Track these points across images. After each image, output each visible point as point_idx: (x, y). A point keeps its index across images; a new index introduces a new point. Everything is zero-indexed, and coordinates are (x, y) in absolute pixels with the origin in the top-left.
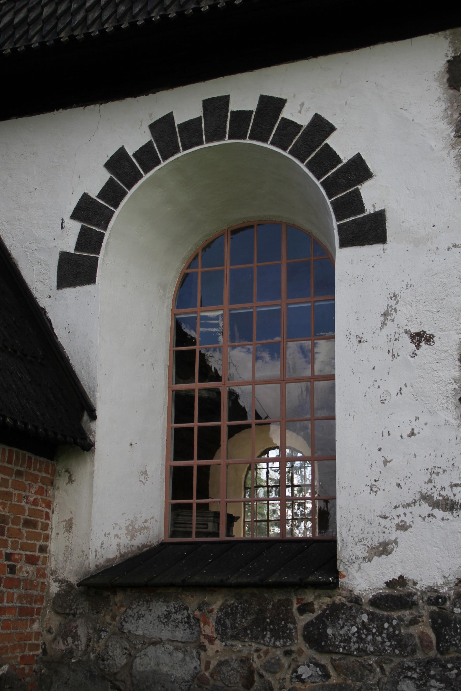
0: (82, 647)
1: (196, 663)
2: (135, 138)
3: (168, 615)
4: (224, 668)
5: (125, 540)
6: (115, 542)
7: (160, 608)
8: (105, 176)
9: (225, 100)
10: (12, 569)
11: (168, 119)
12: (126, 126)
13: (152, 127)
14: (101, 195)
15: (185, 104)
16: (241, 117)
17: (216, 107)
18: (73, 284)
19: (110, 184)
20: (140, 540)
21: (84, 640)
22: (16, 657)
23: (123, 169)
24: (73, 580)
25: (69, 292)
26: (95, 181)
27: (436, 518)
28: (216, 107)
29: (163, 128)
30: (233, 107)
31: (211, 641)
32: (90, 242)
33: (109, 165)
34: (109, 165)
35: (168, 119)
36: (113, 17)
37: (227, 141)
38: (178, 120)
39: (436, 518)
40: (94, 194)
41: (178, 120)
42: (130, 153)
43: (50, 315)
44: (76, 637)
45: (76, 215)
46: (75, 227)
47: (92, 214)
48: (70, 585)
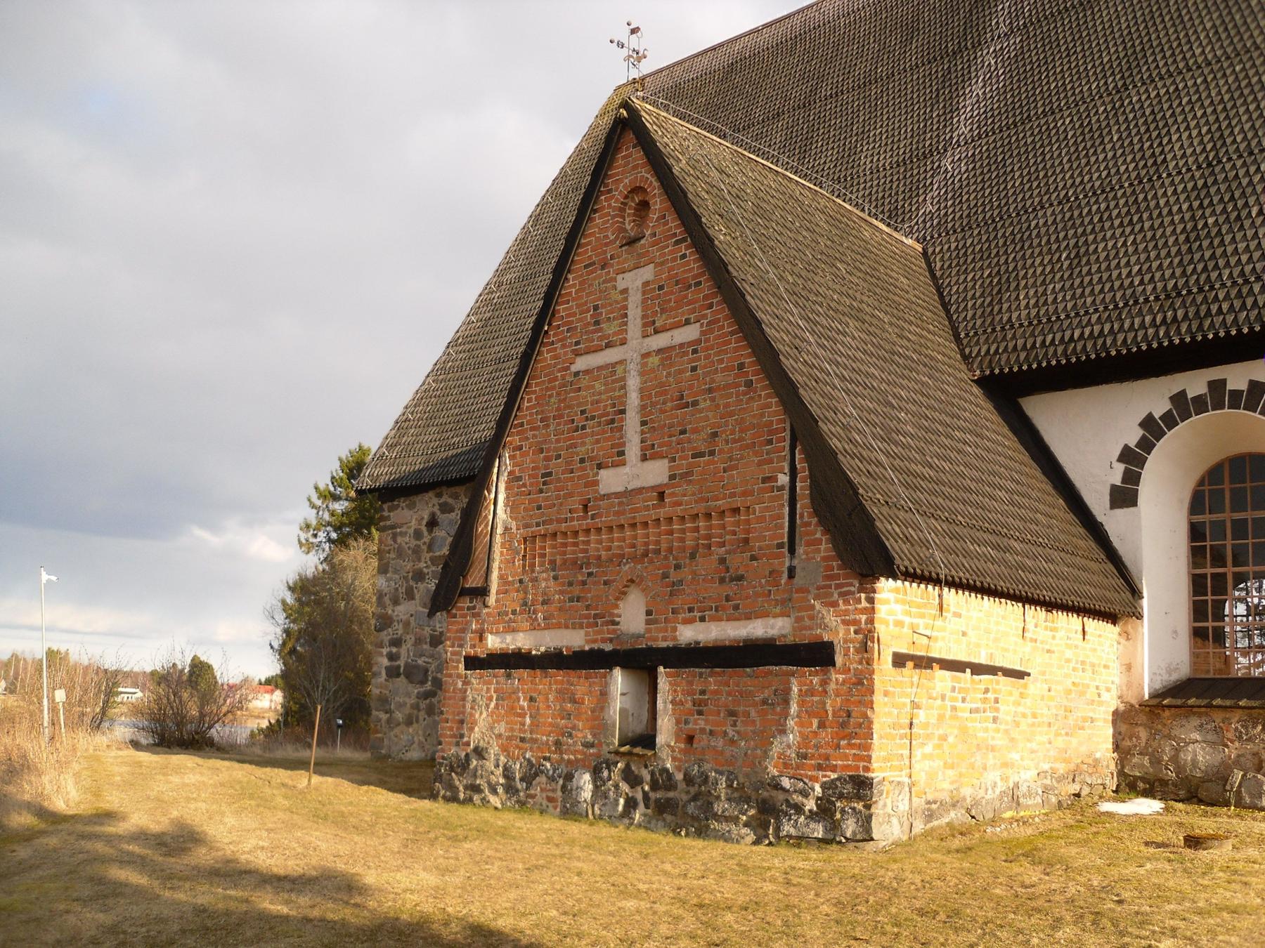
0: (1143, 744)
1: (1222, 755)
2: (1160, 408)
3: (1201, 726)
4: (1242, 759)
5: (1166, 677)
6: (1159, 678)
7: (1195, 721)
8: (1138, 433)
9: (1224, 382)
10: (1099, 695)
11: (1183, 394)
12: (1152, 396)
13: (1171, 398)
14: (1138, 445)
15: (1195, 383)
16: (1236, 394)
17: (1217, 386)
18: (1121, 507)
19: (1143, 438)
20: (1175, 677)
21: (1144, 740)
22: (707, 721)
23: (1153, 429)
24: (1134, 702)
25: (1119, 512)
26: (1133, 436)
27: (1029, 675)
28: (1217, 386)
29: (1179, 399)
30: (1230, 387)
31: (1232, 742)
32: (1132, 478)
33: (1142, 425)
34: (1142, 425)
35: (1183, 394)
36: (98, 829)
37: (1226, 410)
38: (1190, 395)
39: (1029, 675)
40: (1132, 445)
41: (1190, 395)
42: (1157, 416)
43: (1106, 528)
44: (1138, 738)
45: (1120, 460)
46: (1120, 468)
47: (1133, 459)
48: (1132, 706)
